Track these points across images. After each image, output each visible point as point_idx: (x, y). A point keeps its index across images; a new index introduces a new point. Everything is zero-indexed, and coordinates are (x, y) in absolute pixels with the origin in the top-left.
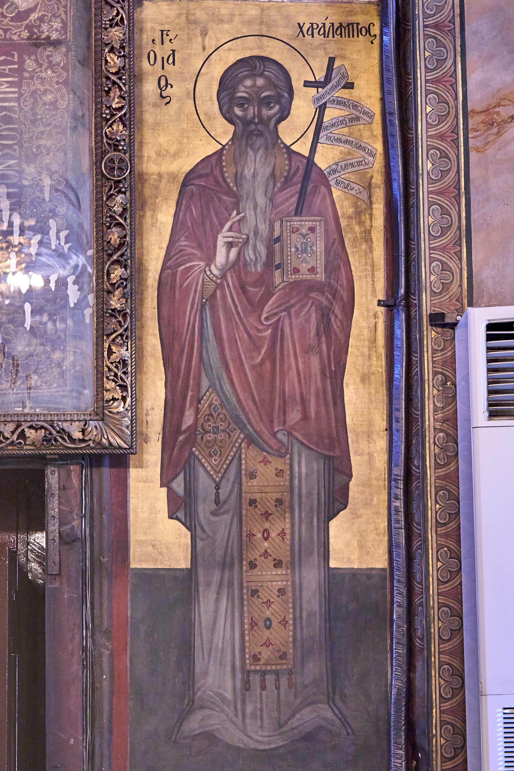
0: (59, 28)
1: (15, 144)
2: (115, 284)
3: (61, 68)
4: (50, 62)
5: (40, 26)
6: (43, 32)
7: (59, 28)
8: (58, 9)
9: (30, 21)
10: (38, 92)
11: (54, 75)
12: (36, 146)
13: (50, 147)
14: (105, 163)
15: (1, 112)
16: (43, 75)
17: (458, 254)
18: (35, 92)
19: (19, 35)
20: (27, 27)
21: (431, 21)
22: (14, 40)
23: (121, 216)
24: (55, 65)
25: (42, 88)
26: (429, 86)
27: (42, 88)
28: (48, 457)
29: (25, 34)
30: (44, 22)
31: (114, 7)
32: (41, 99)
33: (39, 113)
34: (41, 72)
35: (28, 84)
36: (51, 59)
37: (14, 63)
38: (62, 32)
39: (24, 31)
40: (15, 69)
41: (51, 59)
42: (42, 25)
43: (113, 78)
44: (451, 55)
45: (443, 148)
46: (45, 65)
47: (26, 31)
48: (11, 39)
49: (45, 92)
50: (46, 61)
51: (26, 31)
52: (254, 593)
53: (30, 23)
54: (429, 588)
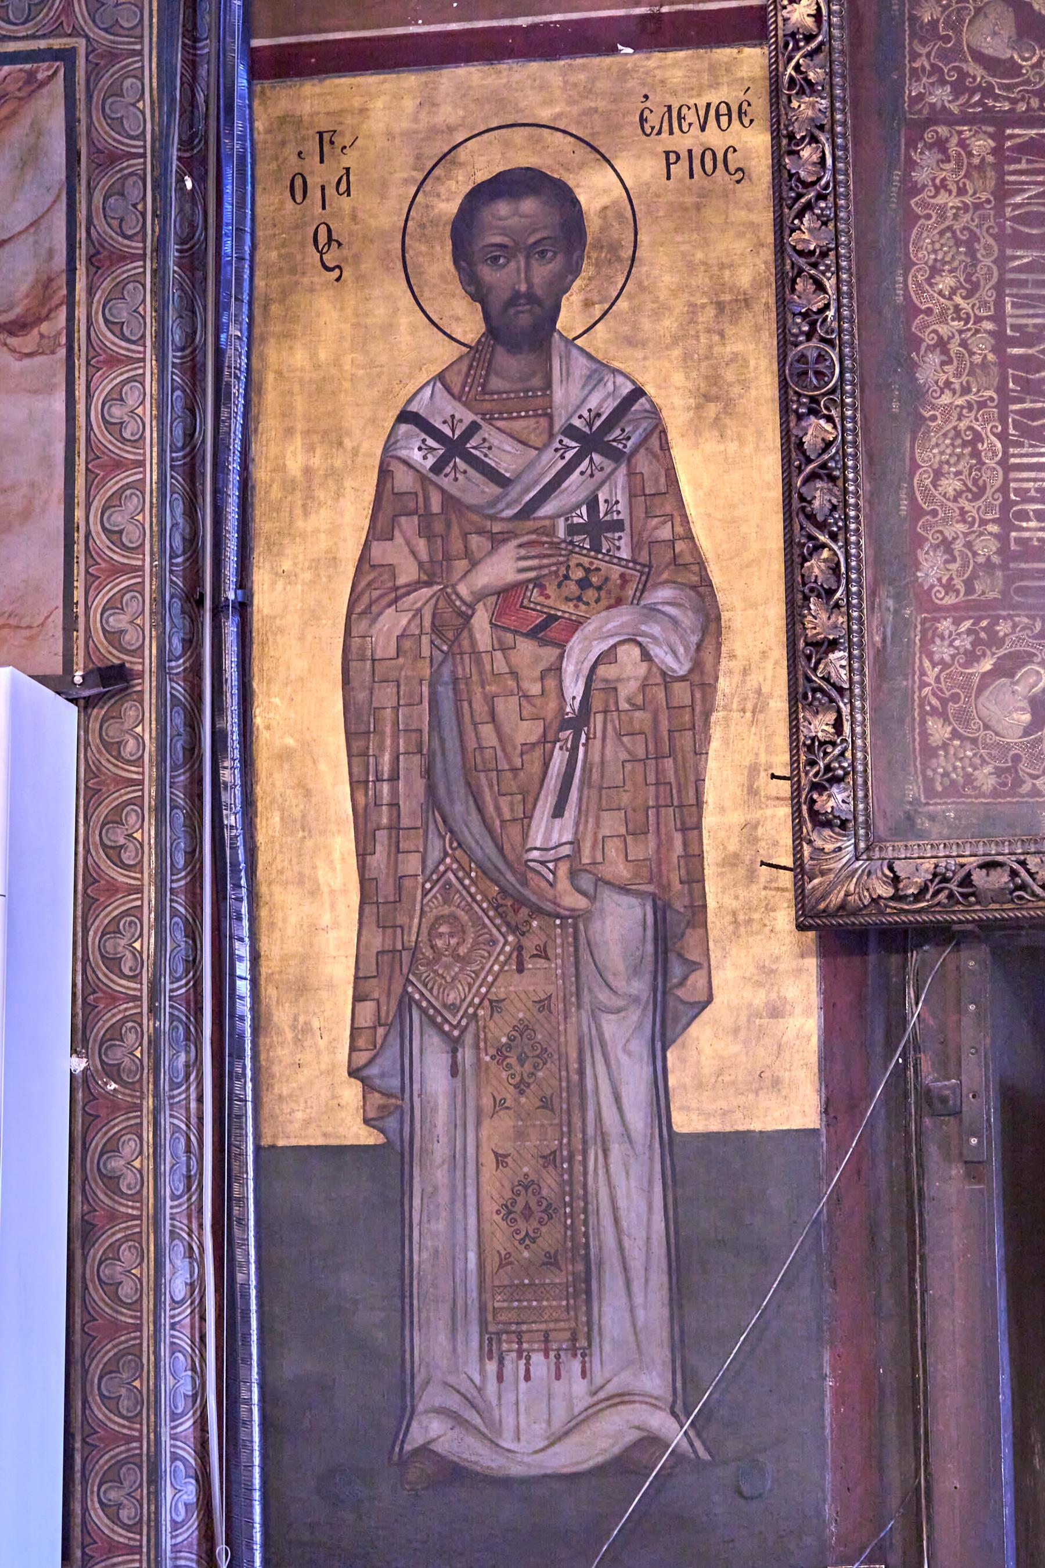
0: (938, 641)
1: (1017, 503)
2: (810, 143)
3: (927, 539)
4: (945, 352)
5: (974, 644)
6: (969, 632)
7: (938, 641)
8: (937, 679)
9: (994, 654)
10: (964, 293)
11: (935, 327)
12: (966, 192)
13: (947, 594)
14: (833, 374)
15: (1043, 425)
16: (961, 527)
17: (88, 1540)
18: (976, 497)
19: (1015, 626)
20: (1000, 643)
21: (131, 477)
22: (1027, 616)
23: (801, 271)
24: (938, 546)
25: (963, 502)
26: (139, 352)
27: (958, 299)
28: (956, 927)
29: (1003, 628)
30: (966, 652)
31: (823, 678)
32: (965, 484)
33: (963, 257)
34: (960, 332)
35: (989, 508)
36: (946, 557)
37: (1015, 412)
38: (930, 634)
39: (1006, 635)
40: (1010, 163)
41: (946, 557)
42: (969, 647)
43: (823, 538)
44: (92, 1162)
45: (116, 1419)
46: (958, 546)
47: (1001, 634)
48: (1033, 618)
49: (958, 494)
50: (956, 553)
51: (1001, 634)
52: (546, 1104)
53: (994, 649)
54: (158, 37)
